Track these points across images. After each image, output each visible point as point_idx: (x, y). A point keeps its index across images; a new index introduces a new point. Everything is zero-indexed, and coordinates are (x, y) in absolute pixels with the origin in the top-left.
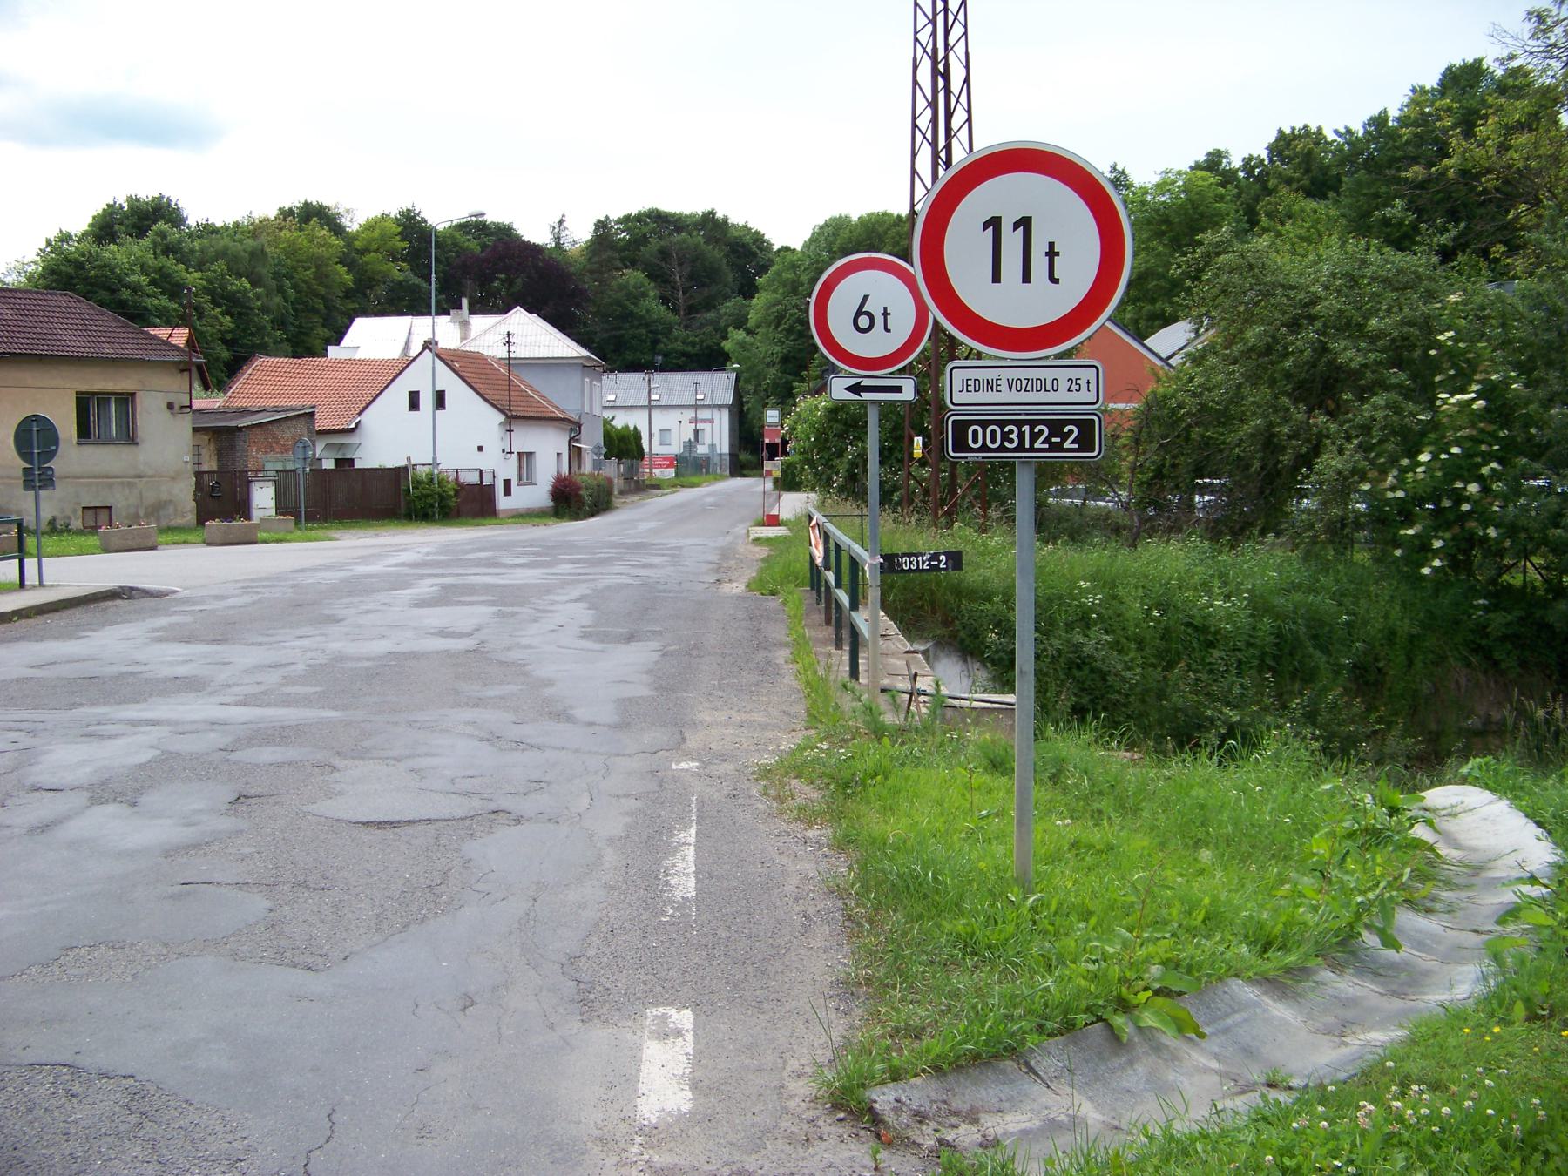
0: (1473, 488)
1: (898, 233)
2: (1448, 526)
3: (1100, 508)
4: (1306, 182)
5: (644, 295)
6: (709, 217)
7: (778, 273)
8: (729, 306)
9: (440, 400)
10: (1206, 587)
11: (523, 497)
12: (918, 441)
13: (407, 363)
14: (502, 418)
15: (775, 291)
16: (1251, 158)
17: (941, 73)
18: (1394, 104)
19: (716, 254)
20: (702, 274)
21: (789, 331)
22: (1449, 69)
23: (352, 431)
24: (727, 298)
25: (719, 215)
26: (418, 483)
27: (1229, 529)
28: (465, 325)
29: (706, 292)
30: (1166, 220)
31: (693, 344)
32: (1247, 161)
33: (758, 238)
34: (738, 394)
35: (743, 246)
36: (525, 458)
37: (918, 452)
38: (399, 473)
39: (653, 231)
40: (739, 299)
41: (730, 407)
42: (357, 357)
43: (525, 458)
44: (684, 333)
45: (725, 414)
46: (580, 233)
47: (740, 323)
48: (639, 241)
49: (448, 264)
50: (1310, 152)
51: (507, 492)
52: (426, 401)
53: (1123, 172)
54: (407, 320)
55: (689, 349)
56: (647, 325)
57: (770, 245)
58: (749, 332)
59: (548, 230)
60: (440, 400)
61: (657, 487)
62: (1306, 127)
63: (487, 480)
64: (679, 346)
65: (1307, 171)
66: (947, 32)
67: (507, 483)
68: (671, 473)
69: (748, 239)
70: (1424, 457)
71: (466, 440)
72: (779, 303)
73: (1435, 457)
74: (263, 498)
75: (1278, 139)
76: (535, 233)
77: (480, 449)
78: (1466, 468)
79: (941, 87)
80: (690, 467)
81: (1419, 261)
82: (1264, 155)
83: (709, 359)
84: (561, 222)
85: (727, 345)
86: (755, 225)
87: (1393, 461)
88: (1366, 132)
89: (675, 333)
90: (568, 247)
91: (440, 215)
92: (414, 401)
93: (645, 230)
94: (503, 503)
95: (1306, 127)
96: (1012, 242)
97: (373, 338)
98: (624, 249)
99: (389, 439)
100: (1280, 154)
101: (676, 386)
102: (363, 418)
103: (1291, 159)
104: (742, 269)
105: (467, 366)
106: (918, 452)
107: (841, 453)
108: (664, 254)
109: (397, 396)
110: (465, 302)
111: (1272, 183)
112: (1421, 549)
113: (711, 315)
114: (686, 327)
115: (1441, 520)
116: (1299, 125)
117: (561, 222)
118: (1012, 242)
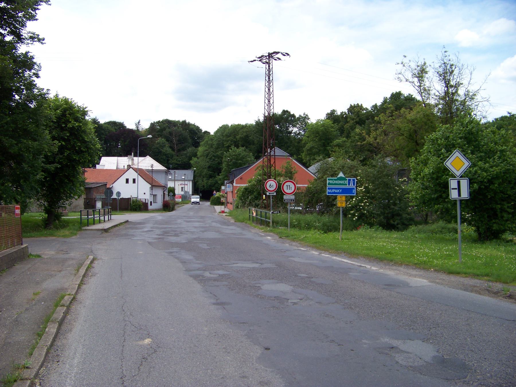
0: (362, 204)
1: (243, 131)
2: (358, 211)
3: (333, 260)
4: (358, 120)
5: (165, 146)
6: (184, 122)
7: (207, 141)
8: (190, 150)
10: (315, 222)
12: (264, 196)
13: (124, 172)
14: (150, 186)
15: (206, 147)
16: (343, 112)
18: (379, 102)
19: (186, 134)
20: (182, 140)
21: (210, 159)
22: (393, 93)
24: (189, 147)
25: (187, 122)
26: (133, 202)
27: (321, 213)
29: (183, 145)
30: (318, 133)
31: (179, 161)
32: (342, 113)
33: (198, 128)
34: (194, 177)
35: (193, 131)
36: (155, 196)
37: (264, 198)
38: (129, 199)
39: (167, 126)
40: (193, 148)
41: (192, 181)
42: (105, 168)
43: (155, 196)
44: (176, 157)
45: (191, 183)
46: (145, 125)
47: (195, 155)
48: (162, 130)
49: (106, 135)
50: (359, 111)
51: (151, 205)
52: (131, 181)
53: (307, 115)
55: (178, 163)
56: (166, 155)
57: (201, 130)
58: (198, 158)
59: (135, 125)
61: (178, 204)
62: (358, 104)
64: (175, 161)
65: (358, 116)
67: (151, 202)
68: (180, 200)
69: (195, 129)
70: (354, 199)
71: (141, 191)
72: (206, 150)
73: (356, 199)
74: (99, 205)
75: (350, 107)
76: (130, 125)
78: (361, 201)
80: (185, 198)
81: (355, 163)
82: (346, 111)
83: (185, 166)
84: (139, 122)
85: (192, 162)
86: (197, 124)
87: (349, 200)
88: (372, 109)
89: (174, 157)
90: (140, 130)
92: (127, 181)
93: (164, 126)
94: (150, 207)
95: (358, 104)
98: (158, 132)
99: (123, 189)
100: (351, 111)
101: (180, 173)
102: (114, 185)
103: (354, 113)
104: (193, 138)
105: (140, 172)
106: (264, 198)
107: (248, 198)
108: (171, 134)
109: (123, 179)
110: (133, 154)
111: (348, 120)
112: (354, 215)
113: (185, 152)
114: (177, 156)
115: (357, 211)
116: (356, 104)
117: (139, 122)
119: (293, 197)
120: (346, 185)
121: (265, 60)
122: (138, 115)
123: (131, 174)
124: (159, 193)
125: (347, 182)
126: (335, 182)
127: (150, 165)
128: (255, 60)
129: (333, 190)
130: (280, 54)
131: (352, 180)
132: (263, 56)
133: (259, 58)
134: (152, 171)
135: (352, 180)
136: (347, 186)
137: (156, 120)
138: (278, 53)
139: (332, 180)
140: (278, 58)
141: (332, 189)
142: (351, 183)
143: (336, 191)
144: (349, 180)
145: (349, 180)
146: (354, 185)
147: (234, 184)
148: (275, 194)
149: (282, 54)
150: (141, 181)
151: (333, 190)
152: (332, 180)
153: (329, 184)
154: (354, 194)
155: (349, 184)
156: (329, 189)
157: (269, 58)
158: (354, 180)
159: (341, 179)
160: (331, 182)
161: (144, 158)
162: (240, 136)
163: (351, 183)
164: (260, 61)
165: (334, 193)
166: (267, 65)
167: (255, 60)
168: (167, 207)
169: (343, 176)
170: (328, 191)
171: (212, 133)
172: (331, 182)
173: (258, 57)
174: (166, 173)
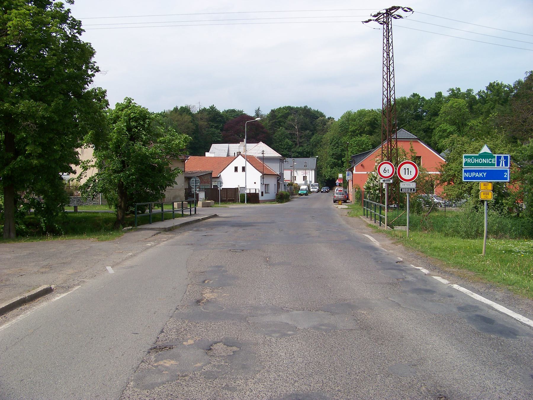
9: (244, 169)
11: (266, 197)
14: (261, 174)
17: (389, 84)
23: (218, 177)
28: (245, 146)
43: (267, 186)
45: (313, 172)
48: (285, 116)
51: (262, 195)
52: (240, 169)
54: (227, 145)
60: (244, 169)
63: (257, 192)
66: (389, 62)
67: (262, 193)
71: (251, 181)
77: (255, 183)
79: (389, 86)
91: (221, 108)
92: (236, 169)
94: (261, 198)
96: (407, 171)
97: (218, 150)
99: (229, 179)
105: (250, 159)
109: (231, 167)
118: (407, 171)
119: (413, 185)
120: (494, 165)
121: (382, 20)
122: (257, 100)
123: (240, 162)
124: (272, 182)
125: (494, 161)
126: (475, 161)
127: (261, 152)
128: (370, 20)
129: (473, 174)
130: (400, 9)
131: (502, 158)
132: (379, 14)
133: (375, 16)
134: (263, 159)
135: (502, 158)
136: (496, 168)
137: (276, 107)
138: (399, 8)
139: (470, 157)
140: (398, 16)
141: (470, 171)
142: (502, 160)
143: (477, 175)
144: (499, 158)
145: (499, 158)
146: (506, 165)
147: (354, 172)
148: (391, 181)
149: (403, 9)
150: (250, 168)
151: (473, 174)
152: (470, 157)
153: (466, 164)
154: (506, 179)
155: (498, 164)
156: (466, 171)
157: (387, 16)
158: (506, 158)
159: (485, 156)
160: (469, 161)
161: (256, 144)
162: (366, 119)
163: (502, 160)
164: (376, 20)
165: (474, 178)
166: (385, 25)
167: (370, 20)
168: (281, 198)
169: (489, 151)
170: (464, 175)
171: (336, 120)
172: (469, 161)
173: (373, 15)
174: (281, 160)
